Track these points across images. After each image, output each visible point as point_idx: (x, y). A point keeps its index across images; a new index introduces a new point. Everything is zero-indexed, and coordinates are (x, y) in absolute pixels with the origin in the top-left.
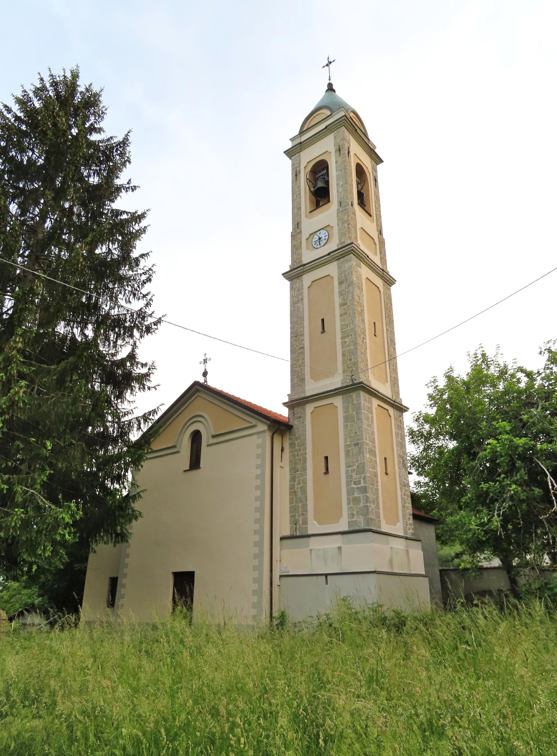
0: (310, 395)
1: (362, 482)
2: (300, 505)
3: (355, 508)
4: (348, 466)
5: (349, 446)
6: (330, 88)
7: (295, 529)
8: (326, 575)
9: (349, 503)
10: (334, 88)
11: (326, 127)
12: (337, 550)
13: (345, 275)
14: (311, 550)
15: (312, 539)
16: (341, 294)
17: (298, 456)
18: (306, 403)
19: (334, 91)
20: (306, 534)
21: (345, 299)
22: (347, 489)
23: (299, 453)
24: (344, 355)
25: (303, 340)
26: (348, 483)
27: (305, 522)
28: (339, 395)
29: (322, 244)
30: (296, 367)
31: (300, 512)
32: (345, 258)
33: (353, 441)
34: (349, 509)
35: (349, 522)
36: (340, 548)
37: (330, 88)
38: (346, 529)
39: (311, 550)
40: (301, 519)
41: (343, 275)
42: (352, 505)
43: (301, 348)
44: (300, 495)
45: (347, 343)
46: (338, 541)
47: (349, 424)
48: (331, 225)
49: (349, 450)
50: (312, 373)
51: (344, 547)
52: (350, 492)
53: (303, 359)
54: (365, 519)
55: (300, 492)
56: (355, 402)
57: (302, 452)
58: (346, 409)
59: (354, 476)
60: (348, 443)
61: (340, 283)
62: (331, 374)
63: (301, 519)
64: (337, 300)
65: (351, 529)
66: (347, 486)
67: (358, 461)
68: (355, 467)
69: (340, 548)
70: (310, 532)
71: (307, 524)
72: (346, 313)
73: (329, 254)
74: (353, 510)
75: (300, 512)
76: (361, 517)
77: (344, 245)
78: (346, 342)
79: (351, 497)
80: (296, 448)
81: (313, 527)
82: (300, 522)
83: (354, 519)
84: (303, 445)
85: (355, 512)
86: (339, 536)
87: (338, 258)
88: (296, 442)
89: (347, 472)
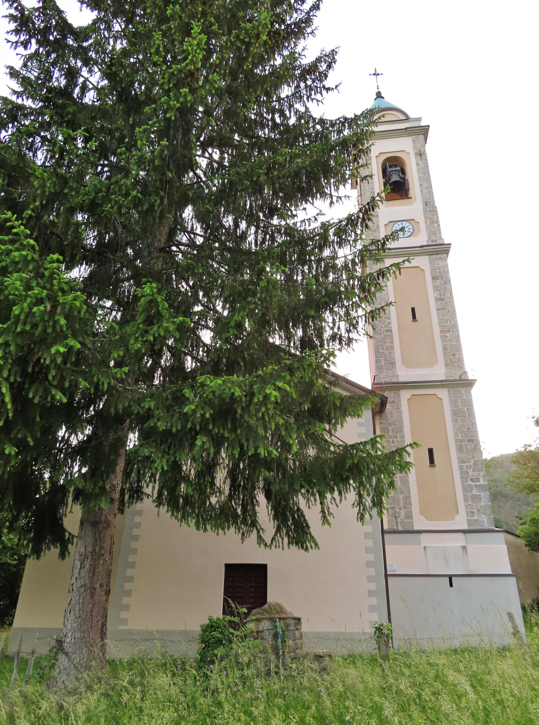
0: (410, 380)
1: (481, 480)
2: (401, 496)
3: (474, 506)
4: (461, 461)
5: (461, 441)
6: (379, 95)
7: (395, 523)
8: (386, 576)
9: (466, 500)
10: (382, 95)
11: (406, 129)
12: (461, 550)
13: (440, 272)
14: (425, 548)
15: (424, 535)
16: (435, 288)
17: (393, 443)
18: (402, 389)
19: (383, 98)
20: (411, 529)
21: (442, 293)
22: (463, 486)
23: (395, 440)
24: (445, 349)
25: (390, 323)
26: (464, 479)
27: (409, 516)
28: (445, 387)
29: (406, 236)
30: (383, 349)
31: (402, 505)
32: (439, 256)
33: (466, 437)
34: (466, 507)
35: (468, 521)
36: (464, 548)
37: (379, 95)
38: (465, 527)
39: (425, 548)
40: (403, 512)
41: (438, 271)
42: (470, 502)
43: (387, 331)
44: (400, 485)
45: (448, 338)
46: (460, 540)
47: (460, 419)
48: (417, 220)
49: (462, 445)
50: (403, 359)
51: (470, 547)
52: (466, 489)
53: (392, 342)
54: (488, 518)
55: (399, 483)
56: (464, 397)
57: (399, 439)
58: (454, 403)
59: (471, 473)
60: (460, 438)
61: (434, 278)
62: (431, 363)
63: (403, 512)
64: (431, 294)
65: (472, 528)
66: (463, 482)
67: (474, 457)
68: (472, 464)
69: (464, 548)
70: (416, 528)
71: (412, 518)
72: (445, 309)
73: (421, 247)
74: (473, 508)
75: (402, 505)
76: (483, 516)
77: (435, 243)
78: (446, 337)
79: (469, 495)
80: (390, 434)
81: (419, 522)
82: (403, 515)
83: (475, 518)
84: (400, 432)
85: (475, 511)
86: (461, 535)
87: (430, 254)
88: (390, 428)
89: (461, 468)
